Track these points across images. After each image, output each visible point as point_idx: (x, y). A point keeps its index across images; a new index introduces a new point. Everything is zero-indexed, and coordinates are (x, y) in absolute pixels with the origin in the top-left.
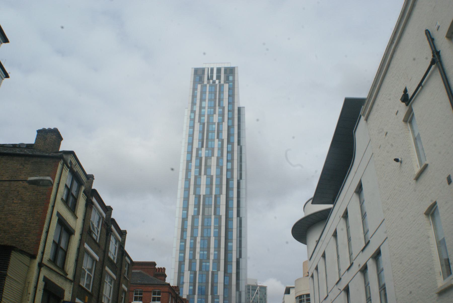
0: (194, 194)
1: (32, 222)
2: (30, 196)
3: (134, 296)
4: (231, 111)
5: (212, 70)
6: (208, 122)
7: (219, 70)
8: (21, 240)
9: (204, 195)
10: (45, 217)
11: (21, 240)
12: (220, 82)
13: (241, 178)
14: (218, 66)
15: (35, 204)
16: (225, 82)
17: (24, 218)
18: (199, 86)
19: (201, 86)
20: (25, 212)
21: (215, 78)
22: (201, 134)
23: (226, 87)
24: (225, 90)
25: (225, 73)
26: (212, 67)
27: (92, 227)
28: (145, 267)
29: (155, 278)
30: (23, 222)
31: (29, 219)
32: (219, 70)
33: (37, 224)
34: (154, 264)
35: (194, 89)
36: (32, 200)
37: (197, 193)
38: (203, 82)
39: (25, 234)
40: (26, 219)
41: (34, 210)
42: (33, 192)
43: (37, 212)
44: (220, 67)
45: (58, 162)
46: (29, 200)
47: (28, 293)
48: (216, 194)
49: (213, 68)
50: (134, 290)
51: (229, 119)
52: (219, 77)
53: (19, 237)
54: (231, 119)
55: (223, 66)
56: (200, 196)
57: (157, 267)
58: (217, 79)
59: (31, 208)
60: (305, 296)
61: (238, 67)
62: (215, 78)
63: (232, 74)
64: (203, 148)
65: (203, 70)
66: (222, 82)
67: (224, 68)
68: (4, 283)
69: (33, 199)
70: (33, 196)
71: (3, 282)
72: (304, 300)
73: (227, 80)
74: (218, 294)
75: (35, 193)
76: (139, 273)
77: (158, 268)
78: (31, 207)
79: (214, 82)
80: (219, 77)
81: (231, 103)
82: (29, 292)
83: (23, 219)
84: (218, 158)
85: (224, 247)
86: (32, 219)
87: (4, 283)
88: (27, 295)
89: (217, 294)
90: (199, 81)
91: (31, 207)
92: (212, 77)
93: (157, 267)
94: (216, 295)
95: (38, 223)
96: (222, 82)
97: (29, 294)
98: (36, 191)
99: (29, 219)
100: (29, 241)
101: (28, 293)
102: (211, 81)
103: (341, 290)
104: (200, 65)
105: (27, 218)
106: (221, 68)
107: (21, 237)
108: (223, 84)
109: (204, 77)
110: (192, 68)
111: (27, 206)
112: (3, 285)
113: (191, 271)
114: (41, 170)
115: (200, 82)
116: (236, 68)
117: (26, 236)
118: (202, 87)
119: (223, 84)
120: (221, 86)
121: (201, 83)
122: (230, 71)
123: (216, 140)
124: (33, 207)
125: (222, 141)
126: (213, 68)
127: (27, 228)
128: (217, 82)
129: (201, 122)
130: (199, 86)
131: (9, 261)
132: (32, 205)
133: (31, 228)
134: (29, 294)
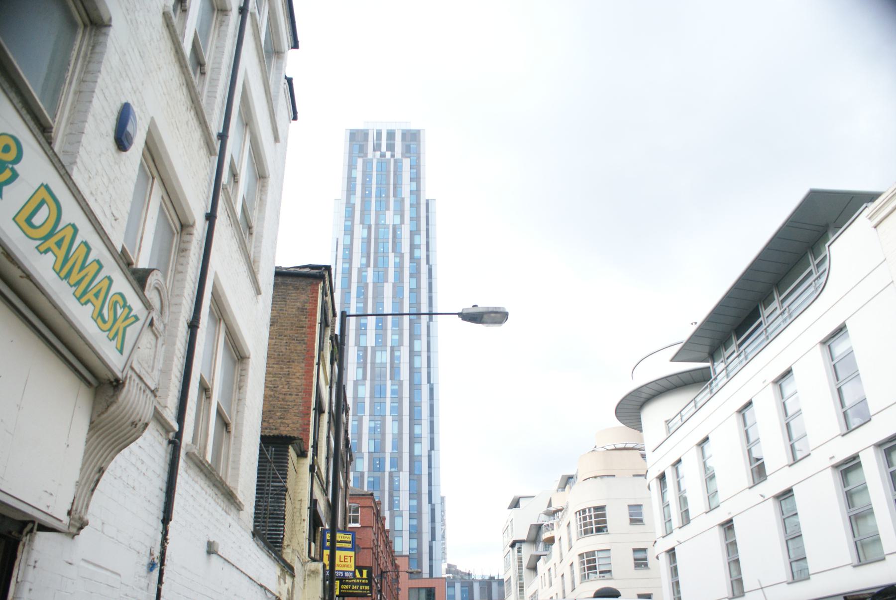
0: (355, 346)
1: (289, 393)
2: (276, 347)
3: (359, 514)
4: (416, 205)
5: (379, 134)
6: (377, 224)
7: (391, 135)
8: (274, 426)
9: (372, 347)
10: (312, 382)
11: (274, 426)
15: (288, 360)
16: (403, 155)
17: (271, 386)
18: (360, 162)
19: (364, 162)
20: (271, 375)
21: (384, 148)
22: (365, 245)
23: (406, 163)
30: (272, 393)
31: (280, 386)
32: (391, 135)
33: (297, 395)
35: (351, 166)
36: (281, 354)
37: (362, 344)
38: (366, 155)
39: (279, 414)
40: (274, 387)
41: (289, 371)
42: (281, 339)
43: (294, 375)
44: (393, 128)
45: (317, 284)
46: (276, 354)
47: (302, 519)
48: (393, 345)
49: (381, 130)
51: (411, 219)
53: (267, 420)
54: (416, 219)
55: (398, 128)
56: (366, 348)
58: (387, 150)
59: (281, 368)
60: (592, 509)
61: (424, 130)
62: (384, 148)
63: (416, 141)
64: (368, 268)
65: (365, 134)
66: (398, 155)
67: (401, 131)
68: (284, 504)
69: (282, 352)
70: (281, 346)
71: (282, 503)
73: (407, 151)
74: (401, 509)
75: (285, 341)
78: (282, 366)
79: (383, 155)
80: (391, 147)
81: (416, 193)
82: (303, 518)
83: (270, 387)
84: (394, 285)
86: (287, 387)
87: (284, 504)
88: (301, 523)
89: (399, 508)
90: (359, 152)
91: (282, 366)
94: (397, 509)
95: (300, 394)
96: (398, 155)
97: (304, 520)
98: (285, 336)
99: (280, 386)
100: (288, 426)
101: (302, 519)
102: (378, 153)
103: (764, 497)
104: (359, 126)
105: (278, 386)
106: (368, 130)
107: (271, 421)
109: (367, 145)
110: (346, 130)
111: (274, 364)
112: (283, 508)
113: (356, 471)
114: (288, 299)
115: (362, 155)
116: (421, 131)
117: (281, 418)
118: (364, 163)
121: (362, 157)
122: (412, 138)
123: (391, 255)
124: (285, 366)
125: (401, 256)
126: (381, 130)
127: (279, 403)
128: (388, 154)
129: (365, 223)
130: (360, 162)
131: (286, 465)
132: (282, 361)
133: (288, 403)
134: (304, 520)
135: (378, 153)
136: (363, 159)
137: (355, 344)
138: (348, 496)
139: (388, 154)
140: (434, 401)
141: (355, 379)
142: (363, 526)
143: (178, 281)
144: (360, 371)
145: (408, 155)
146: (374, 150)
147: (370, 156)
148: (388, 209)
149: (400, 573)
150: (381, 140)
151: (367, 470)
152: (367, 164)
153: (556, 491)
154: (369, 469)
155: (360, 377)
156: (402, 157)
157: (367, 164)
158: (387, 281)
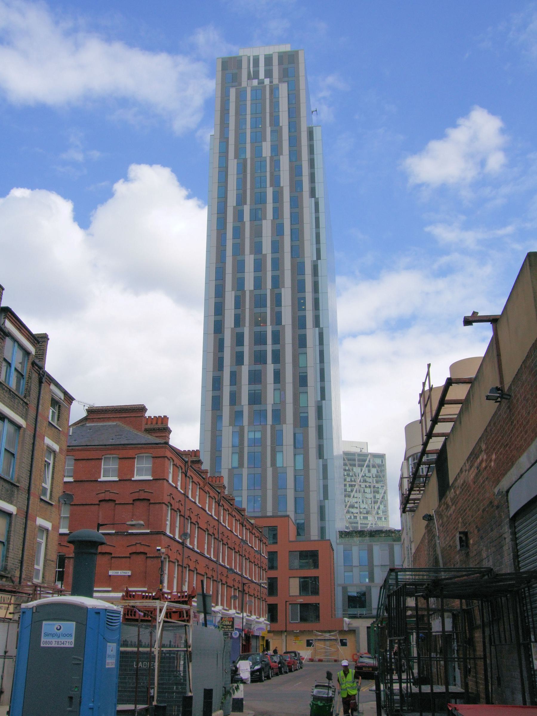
3: (102, 467)
5: (256, 60)
7: (268, 59)
12: (271, 82)
13: (319, 257)
14: (267, 53)
16: (281, 81)
18: (233, 92)
21: (262, 75)
23: (283, 89)
24: (280, 96)
25: (280, 63)
26: (256, 54)
27: (102, 424)
28: (125, 416)
29: (245, 654)
34: (142, 409)
38: (240, 84)
50: (103, 458)
52: (269, 74)
57: (147, 415)
62: (262, 75)
66: (276, 81)
72: (175, 709)
76: (116, 426)
77: (150, 417)
85: (291, 342)
92: (256, 75)
93: (147, 415)
96: (276, 81)
108: (278, 85)
119: (278, 85)
120: (274, 90)
130: (233, 92)
135: (255, 82)
136: (236, 89)
137: (230, 423)
138: (50, 502)
139: (267, 81)
140: (325, 364)
141: (230, 467)
142: (121, 479)
143: (4, 601)
144: (236, 457)
145: (286, 79)
146: (249, 78)
147: (244, 84)
148: (265, 140)
149: (8, 624)
150: (258, 67)
151: (250, 157)
152: (241, 96)
153: (245, 685)
154: (249, 423)
155: (236, 464)
156: (279, 82)
157: (241, 96)
158: (265, 219)
